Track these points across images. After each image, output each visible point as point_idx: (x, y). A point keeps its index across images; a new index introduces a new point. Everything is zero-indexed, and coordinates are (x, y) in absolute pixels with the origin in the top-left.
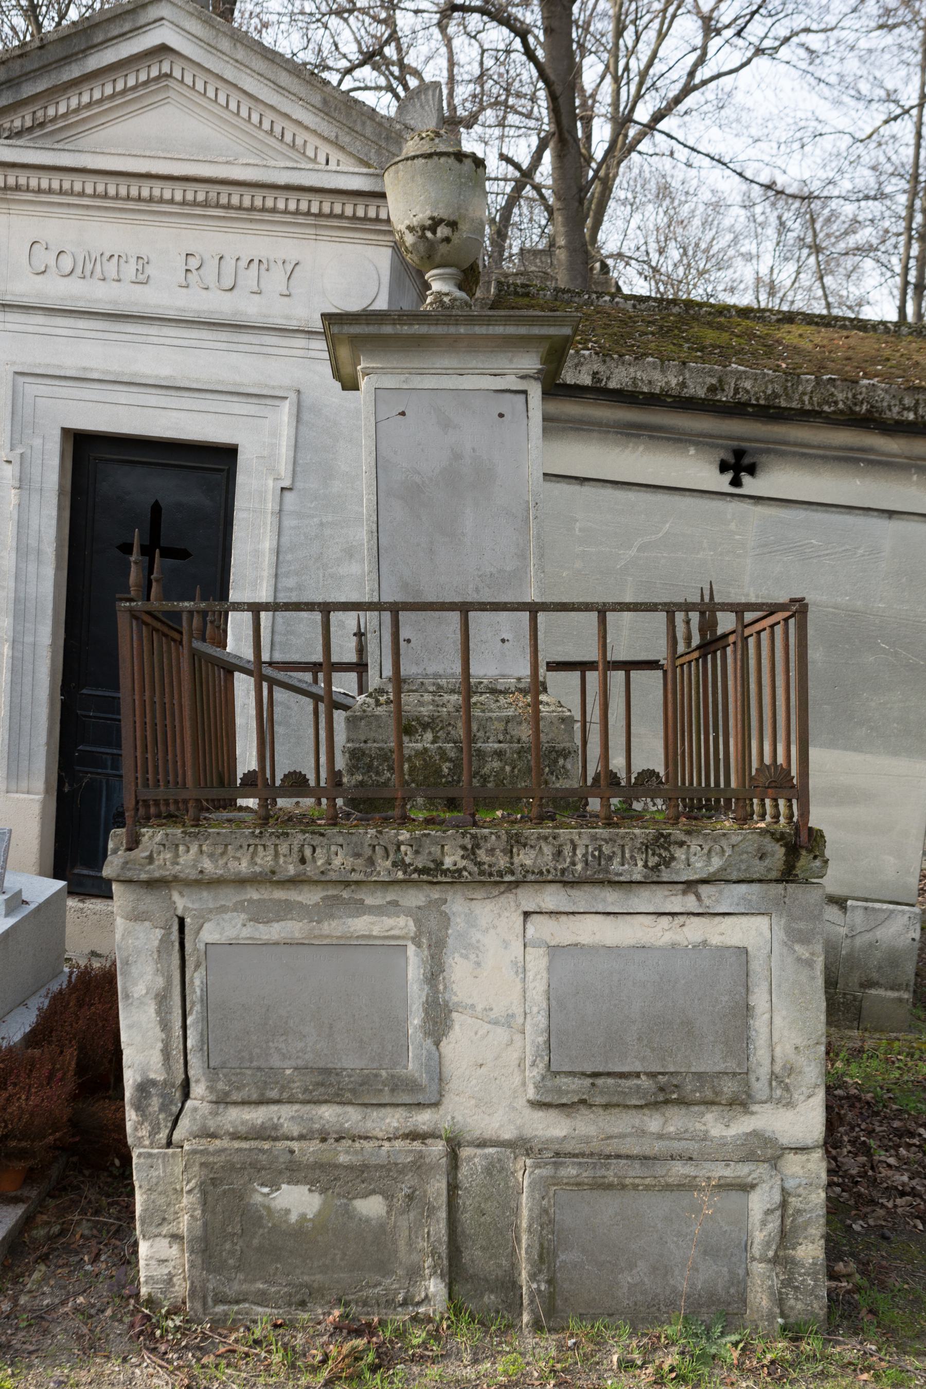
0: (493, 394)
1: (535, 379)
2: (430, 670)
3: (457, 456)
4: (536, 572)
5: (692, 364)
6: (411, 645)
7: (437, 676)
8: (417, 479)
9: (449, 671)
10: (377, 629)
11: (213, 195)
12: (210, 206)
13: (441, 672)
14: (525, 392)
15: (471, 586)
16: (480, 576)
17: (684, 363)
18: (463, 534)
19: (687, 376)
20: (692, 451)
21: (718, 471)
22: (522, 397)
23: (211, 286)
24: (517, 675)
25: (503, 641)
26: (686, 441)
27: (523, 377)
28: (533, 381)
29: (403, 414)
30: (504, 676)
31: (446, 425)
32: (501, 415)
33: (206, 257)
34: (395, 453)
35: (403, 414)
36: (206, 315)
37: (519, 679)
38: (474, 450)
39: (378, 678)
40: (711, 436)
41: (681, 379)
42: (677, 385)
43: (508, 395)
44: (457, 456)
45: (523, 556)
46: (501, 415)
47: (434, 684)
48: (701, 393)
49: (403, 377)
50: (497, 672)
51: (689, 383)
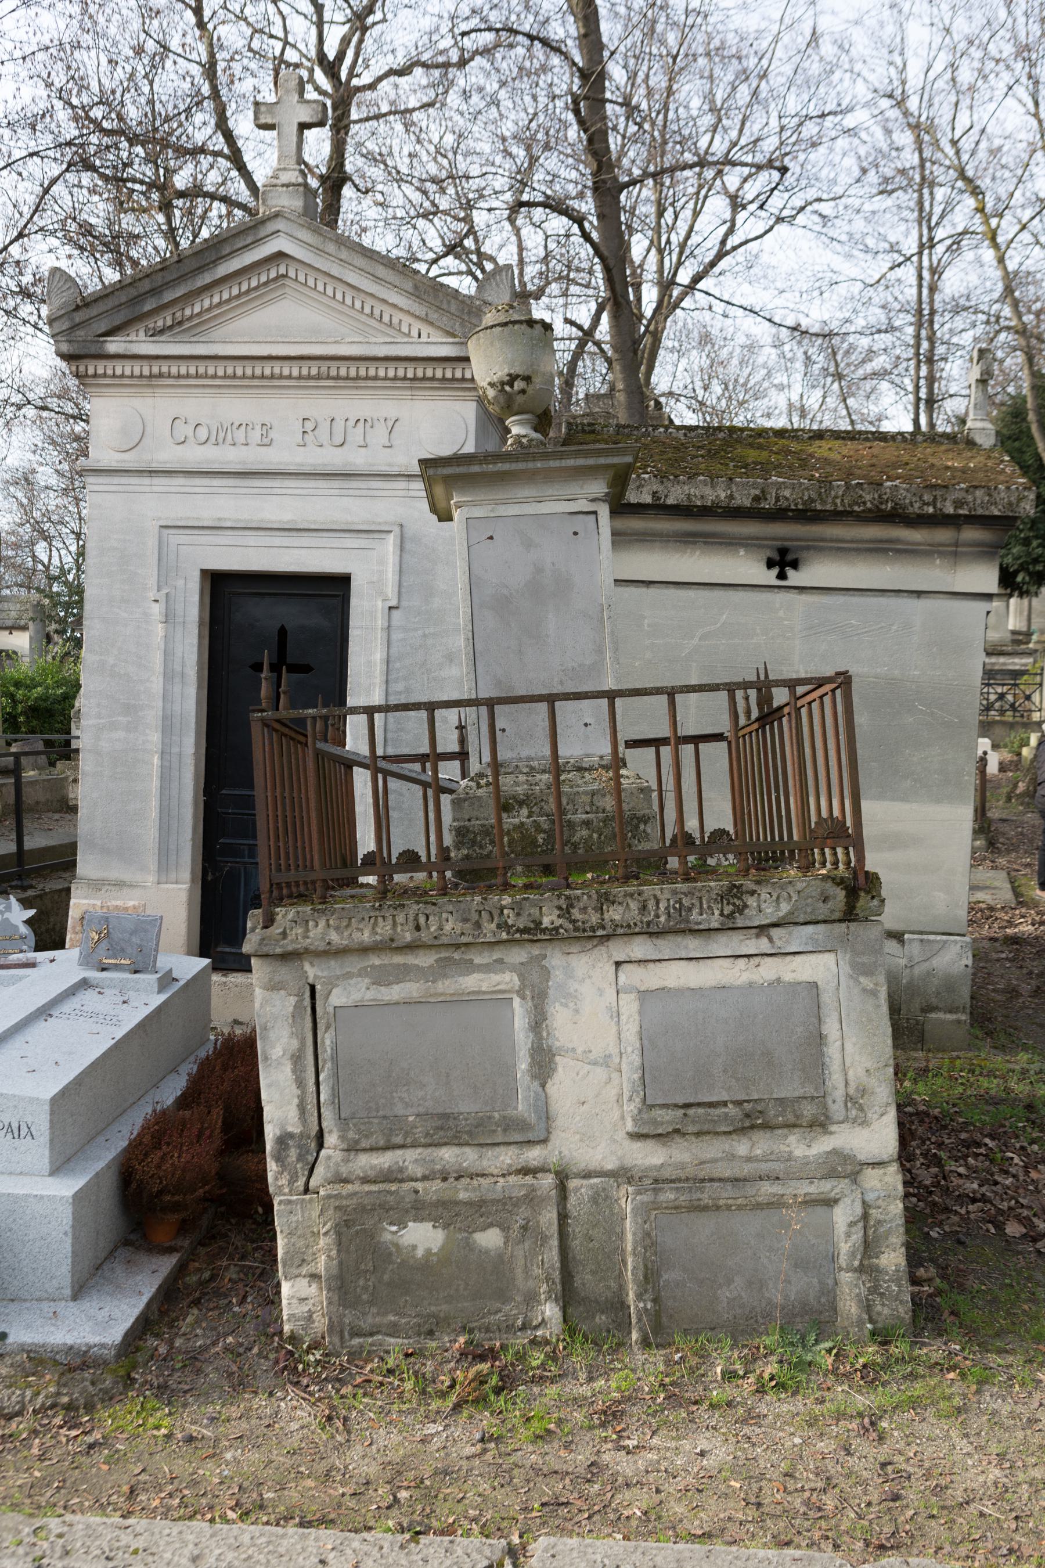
2: (523, 755)
3: (539, 570)
7: (529, 759)
8: (505, 592)
11: (324, 369)
14: (595, 513)
17: (731, 479)
18: (547, 636)
24: (599, 754)
25: (586, 725)
27: (593, 500)
29: (491, 538)
30: (588, 756)
31: (529, 545)
32: (575, 533)
35: (491, 538)
37: (601, 757)
43: (581, 516)
44: (539, 570)
45: (600, 651)
46: (575, 533)
48: (747, 503)
49: (490, 507)
50: (581, 752)
51: (736, 495)
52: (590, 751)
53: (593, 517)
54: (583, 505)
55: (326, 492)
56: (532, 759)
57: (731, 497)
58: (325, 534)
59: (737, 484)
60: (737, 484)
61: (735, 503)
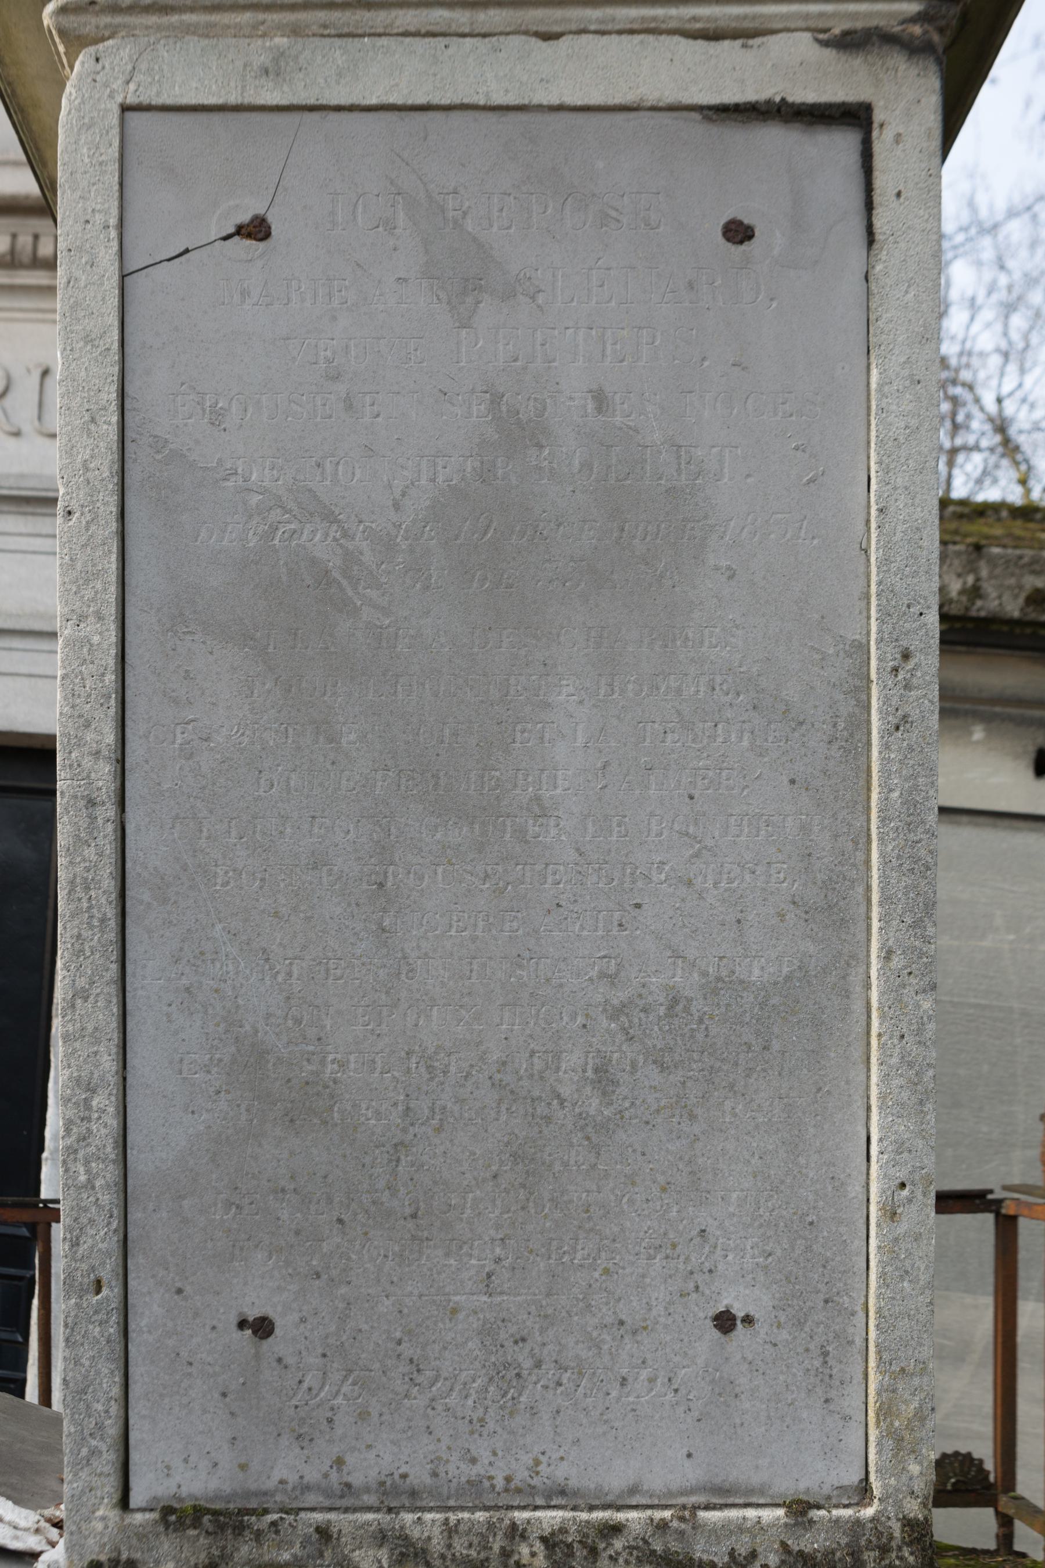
0: (695, 128)
1: (913, 49)
2: (365, 1469)
3: (516, 429)
4: (894, 991)
5: (996, 550)
6: (273, 1346)
7: (397, 1494)
8: (319, 542)
9: (458, 1470)
10: (108, 1271)
11: (25, 241)
12: (21, 266)
13: (419, 1476)
14: (856, 117)
15: (573, 1059)
16: (616, 1013)
17: (978, 548)
18: (540, 809)
19: (984, 573)
20: (978, 733)
21: (1030, 773)
22: (840, 145)
23: (27, 428)
24: (788, 1486)
25: (725, 1322)
26: (966, 713)
27: (851, 42)
28: (898, 61)
29: (256, 230)
30: (724, 1495)
31: (468, 279)
32: (738, 232)
33: (17, 373)
34: (217, 418)
35: (256, 230)
36: (11, 482)
37: (800, 1509)
38: (600, 400)
39: (107, 1511)
40: (1020, 702)
41: (970, 579)
42: (963, 592)
43: (774, 137)
44: (516, 429)
45: (833, 910)
46: (738, 232)
47: (381, 1537)
48: (1013, 608)
49: (259, 52)
50: (692, 1474)
51: (989, 588)
52: (741, 1471)
53: (843, 144)
54: (792, 66)
55: (23, 543)
56: (415, 1499)
57: (975, 592)
58: (16, 643)
59: (992, 562)
60: (992, 562)
61: (982, 608)
